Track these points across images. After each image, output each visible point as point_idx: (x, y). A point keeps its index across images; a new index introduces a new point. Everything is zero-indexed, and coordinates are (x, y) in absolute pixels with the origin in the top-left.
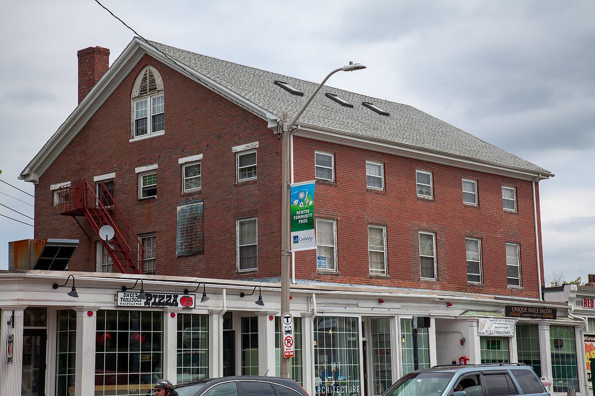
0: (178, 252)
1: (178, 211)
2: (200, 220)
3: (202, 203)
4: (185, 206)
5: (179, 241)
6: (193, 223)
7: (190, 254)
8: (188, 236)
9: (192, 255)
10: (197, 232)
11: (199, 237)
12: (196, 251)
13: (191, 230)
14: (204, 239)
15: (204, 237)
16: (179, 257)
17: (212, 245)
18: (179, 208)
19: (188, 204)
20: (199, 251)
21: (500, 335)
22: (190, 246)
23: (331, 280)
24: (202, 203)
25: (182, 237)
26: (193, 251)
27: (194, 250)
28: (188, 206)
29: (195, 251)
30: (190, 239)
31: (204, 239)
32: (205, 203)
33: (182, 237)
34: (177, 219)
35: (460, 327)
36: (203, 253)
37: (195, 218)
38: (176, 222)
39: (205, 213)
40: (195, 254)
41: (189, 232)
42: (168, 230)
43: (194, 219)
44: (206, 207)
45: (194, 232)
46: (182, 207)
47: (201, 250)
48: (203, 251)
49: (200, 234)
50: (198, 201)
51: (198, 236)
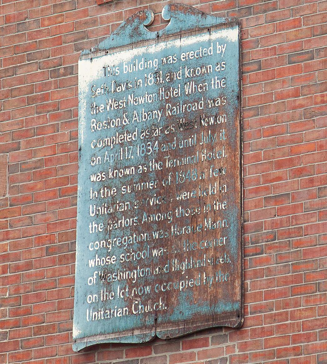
0: (84, 324)
1: (83, 86)
2: (222, 135)
3: (232, 34)
4: (126, 55)
5: (87, 261)
6: (176, 154)
7: (160, 332)
8: (148, 227)
9: (172, 341)
10: (201, 202)
11: (212, 233)
12: (195, 318)
13: (166, 193)
14: (242, 244)
15: (243, 229)
16: (91, 350)
17: (297, 279)
18: (89, 71)
19: (144, 41)
20: (214, 317)
21: (75, 303)
22: (155, 284)
23: (294, 291)
24: (232, 34)
25: (136, 229)
26: (176, 316)
27: (185, 310)
28: (147, 57)
29: (188, 314)
30: (161, 243)
31: (242, 244)
32: (253, 33)
33: (136, 229)
34: (74, 136)
35: (130, 323)
36: (240, 328)
37: (189, 126)
38: (73, 152)
39: (253, 92)
40: (193, 334)
41: (155, 203)
42: (25, 200)
43: (180, 125)
44: (255, 54)
45: (185, 204)
46: (111, 60)
47: (223, 307)
48: (241, 313)
49: (216, 215)
50: (210, 21)
51: (208, 223)
